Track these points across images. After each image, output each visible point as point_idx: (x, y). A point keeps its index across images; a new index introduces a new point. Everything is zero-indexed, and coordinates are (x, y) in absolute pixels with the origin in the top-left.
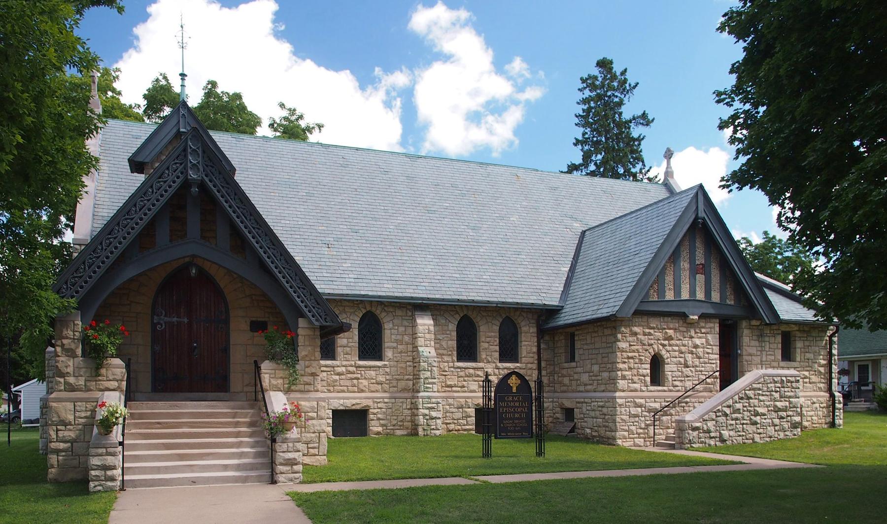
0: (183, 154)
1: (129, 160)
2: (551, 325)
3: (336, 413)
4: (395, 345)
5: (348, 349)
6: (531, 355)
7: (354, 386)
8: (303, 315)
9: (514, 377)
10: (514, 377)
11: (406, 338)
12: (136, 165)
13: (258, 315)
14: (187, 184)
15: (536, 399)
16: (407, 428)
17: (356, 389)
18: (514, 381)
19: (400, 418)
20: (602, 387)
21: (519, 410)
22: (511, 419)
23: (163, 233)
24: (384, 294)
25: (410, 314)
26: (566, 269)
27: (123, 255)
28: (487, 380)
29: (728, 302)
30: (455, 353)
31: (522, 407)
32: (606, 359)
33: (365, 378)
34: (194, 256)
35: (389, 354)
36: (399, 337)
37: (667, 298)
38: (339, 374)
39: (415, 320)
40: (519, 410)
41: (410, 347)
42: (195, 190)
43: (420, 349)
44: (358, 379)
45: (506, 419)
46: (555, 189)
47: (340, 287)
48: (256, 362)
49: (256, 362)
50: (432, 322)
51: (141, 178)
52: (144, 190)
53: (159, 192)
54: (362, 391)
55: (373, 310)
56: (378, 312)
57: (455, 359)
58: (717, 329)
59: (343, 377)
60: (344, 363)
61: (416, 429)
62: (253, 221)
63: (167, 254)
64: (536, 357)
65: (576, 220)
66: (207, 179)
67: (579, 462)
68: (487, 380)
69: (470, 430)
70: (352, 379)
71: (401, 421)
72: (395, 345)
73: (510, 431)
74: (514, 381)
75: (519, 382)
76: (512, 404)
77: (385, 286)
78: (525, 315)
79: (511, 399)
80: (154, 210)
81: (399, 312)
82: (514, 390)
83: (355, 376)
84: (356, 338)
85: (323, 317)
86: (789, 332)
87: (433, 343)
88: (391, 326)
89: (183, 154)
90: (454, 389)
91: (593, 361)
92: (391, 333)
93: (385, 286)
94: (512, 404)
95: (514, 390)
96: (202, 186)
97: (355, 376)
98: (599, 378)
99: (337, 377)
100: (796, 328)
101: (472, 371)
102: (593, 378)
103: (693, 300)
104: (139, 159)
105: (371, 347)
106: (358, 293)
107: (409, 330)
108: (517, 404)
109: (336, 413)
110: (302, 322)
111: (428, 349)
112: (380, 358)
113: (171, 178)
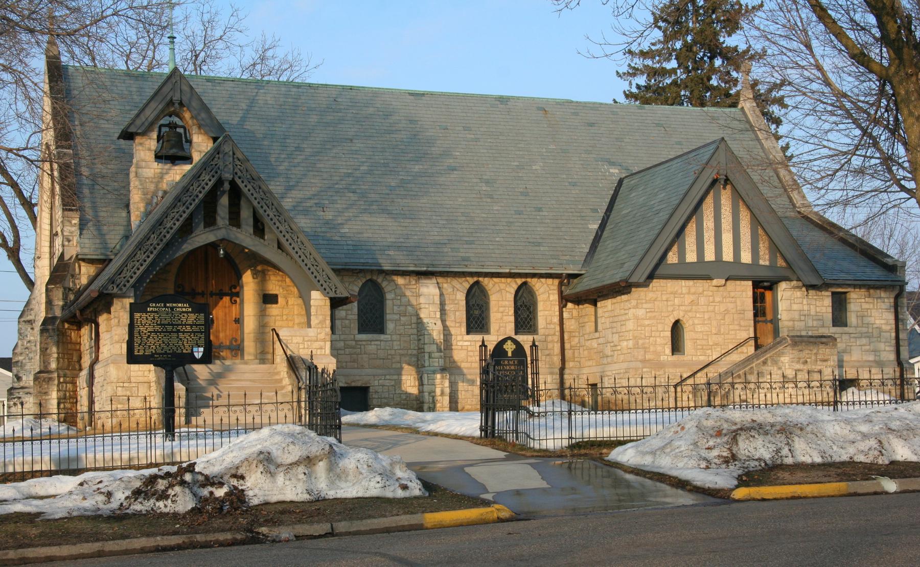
2: (175, 378)
5: (347, 322)
6: (552, 326)
9: (509, 342)
10: (509, 342)
14: (220, 182)
26: (595, 226)
27: (167, 245)
29: (761, 262)
35: (390, 326)
42: (227, 186)
46: (591, 125)
55: (375, 278)
56: (379, 280)
57: (464, 329)
59: (340, 352)
60: (342, 337)
65: (612, 164)
67: (645, 477)
74: (509, 346)
82: (510, 354)
84: (356, 310)
94: (508, 368)
95: (510, 354)
96: (233, 183)
98: (619, 348)
106: (357, 261)
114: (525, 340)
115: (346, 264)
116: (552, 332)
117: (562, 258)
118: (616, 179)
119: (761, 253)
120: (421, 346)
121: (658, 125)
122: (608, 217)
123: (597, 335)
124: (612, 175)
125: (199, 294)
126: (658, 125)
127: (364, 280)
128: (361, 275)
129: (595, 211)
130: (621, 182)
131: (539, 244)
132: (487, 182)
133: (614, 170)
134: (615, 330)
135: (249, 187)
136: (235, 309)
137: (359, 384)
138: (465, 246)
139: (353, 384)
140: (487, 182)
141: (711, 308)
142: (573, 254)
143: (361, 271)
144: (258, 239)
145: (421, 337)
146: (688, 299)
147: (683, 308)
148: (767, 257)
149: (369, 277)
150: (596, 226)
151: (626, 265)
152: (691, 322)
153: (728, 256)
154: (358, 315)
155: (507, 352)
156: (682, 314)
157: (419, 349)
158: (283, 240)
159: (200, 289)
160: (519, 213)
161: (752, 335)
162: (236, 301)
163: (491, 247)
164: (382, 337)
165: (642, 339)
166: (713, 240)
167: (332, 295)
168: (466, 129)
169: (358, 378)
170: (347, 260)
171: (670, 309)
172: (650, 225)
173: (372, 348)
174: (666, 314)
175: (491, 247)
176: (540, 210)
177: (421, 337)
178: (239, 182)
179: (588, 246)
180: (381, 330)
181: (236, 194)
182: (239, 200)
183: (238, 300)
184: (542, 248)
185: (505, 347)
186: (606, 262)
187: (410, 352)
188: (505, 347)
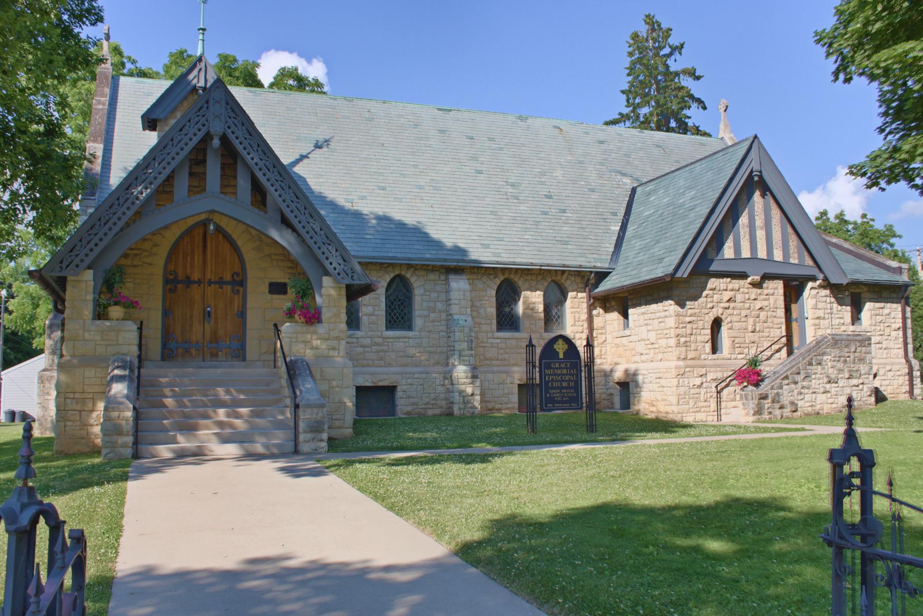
0: (206, 105)
1: (143, 117)
3: (360, 390)
4: (426, 313)
5: (374, 318)
6: (581, 323)
7: (381, 359)
8: (327, 273)
9: (561, 341)
10: (561, 341)
11: (439, 305)
12: (150, 122)
13: (280, 276)
14: (208, 137)
15: (585, 366)
16: (441, 407)
17: (382, 363)
18: (560, 347)
19: (432, 396)
20: (660, 356)
21: (567, 378)
22: (557, 388)
23: (182, 184)
24: (414, 256)
25: (443, 277)
26: (616, 228)
28: (531, 346)
29: (792, 261)
30: (495, 322)
31: (571, 374)
32: (662, 324)
33: (393, 351)
34: (212, 212)
35: (418, 322)
36: (432, 304)
37: (726, 256)
38: (364, 346)
39: (449, 285)
40: (567, 378)
41: (444, 316)
42: (216, 142)
43: (456, 317)
44: (385, 352)
45: (553, 388)
46: (601, 142)
47: (365, 249)
48: (276, 325)
49: (276, 325)
50: (468, 287)
51: (152, 138)
52: (163, 144)
53: (179, 145)
54: (390, 365)
55: (403, 273)
56: (408, 276)
57: (494, 327)
58: (781, 291)
59: (367, 349)
60: (369, 334)
61: (451, 408)
62: (276, 173)
63: (186, 209)
64: (586, 325)
65: (624, 175)
66: (229, 132)
68: (531, 346)
69: (514, 408)
70: (378, 352)
71: (434, 399)
72: (426, 313)
73: (558, 402)
74: (561, 346)
75: (566, 347)
76: (559, 372)
77: (416, 247)
78: (573, 279)
79: (557, 365)
80: (174, 164)
81: (432, 276)
82: (561, 356)
83: (382, 348)
85: (350, 275)
86: (860, 294)
87: (469, 310)
88: (422, 291)
89: (206, 105)
90: (494, 362)
91: (650, 327)
92: (423, 292)
93: (416, 247)
94: (559, 372)
95: (561, 356)
96: (224, 139)
97: (382, 348)
99: (360, 350)
100: (865, 289)
101: (514, 342)
102: (650, 346)
103: (754, 258)
104: (154, 116)
105: (399, 315)
106: (385, 254)
107: (443, 296)
108: (564, 371)
109: (360, 390)
110: (326, 281)
111: (463, 317)
112: (410, 328)
113: (192, 131)
114: (104, 300)
115: (373, 258)
116: (580, 329)
117: (589, 256)
118: (629, 187)
119: (791, 252)
120: (450, 344)
121: (658, 146)
122: (627, 220)
123: (627, 332)
124: (625, 184)
125: (194, 282)
126: (658, 146)
127: (392, 275)
128: (390, 269)
129: (615, 214)
130: (634, 190)
131: (566, 243)
132: (513, 185)
133: (627, 180)
134: (650, 327)
135: (246, 143)
136: (237, 301)
137: (386, 383)
138: (495, 243)
139: (380, 384)
140: (513, 185)
141: (747, 305)
142: (600, 252)
143: (390, 265)
144: (256, 210)
145: (451, 335)
146: (727, 295)
147: (722, 305)
148: (796, 255)
149: (397, 272)
150: (618, 228)
151: (666, 260)
152: (729, 319)
153: (762, 254)
154: (386, 311)
155: (558, 353)
156: (720, 311)
157: (915, 590)
158: (287, 212)
159: (196, 276)
160: (545, 213)
161: (784, 334)
162: (238, 291)
163: (520, 244)
164: (410, 334)
165: (682, 336)
166: (748, 237)
167: (348, 281)
168: (490, 139)
169: (384, 376)
170: (376, 254)
171: (710, 305)
172: (686, 221)
173: (400, 345)
174: (707, 311)
175: (520, 244)
176: (564, 211)
177: (451, 335)
178: (232, 137)
179: (613, 246)
180: (271, 292)
181: (230, 155)
182: (236, 163)
183: (241, 289)
184: (570, 247)
185: (556, 346)
186: (636, 260)
187: (439, 350)
188: (556, 346)
